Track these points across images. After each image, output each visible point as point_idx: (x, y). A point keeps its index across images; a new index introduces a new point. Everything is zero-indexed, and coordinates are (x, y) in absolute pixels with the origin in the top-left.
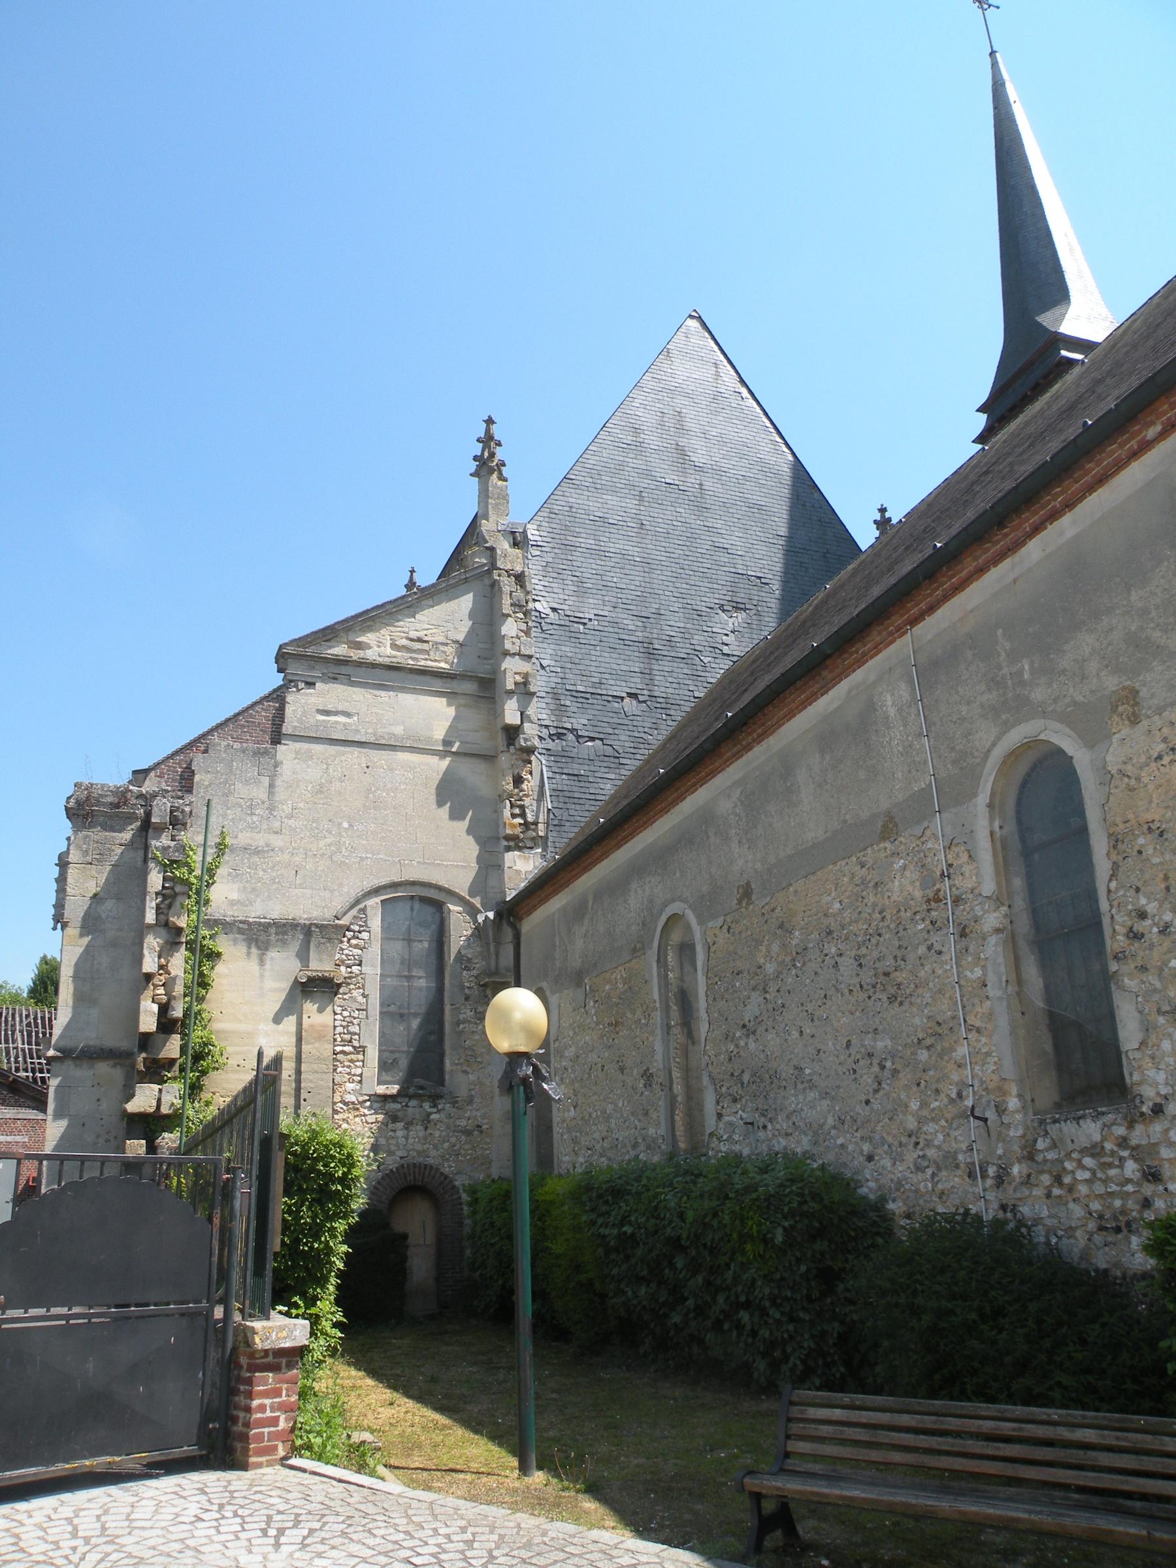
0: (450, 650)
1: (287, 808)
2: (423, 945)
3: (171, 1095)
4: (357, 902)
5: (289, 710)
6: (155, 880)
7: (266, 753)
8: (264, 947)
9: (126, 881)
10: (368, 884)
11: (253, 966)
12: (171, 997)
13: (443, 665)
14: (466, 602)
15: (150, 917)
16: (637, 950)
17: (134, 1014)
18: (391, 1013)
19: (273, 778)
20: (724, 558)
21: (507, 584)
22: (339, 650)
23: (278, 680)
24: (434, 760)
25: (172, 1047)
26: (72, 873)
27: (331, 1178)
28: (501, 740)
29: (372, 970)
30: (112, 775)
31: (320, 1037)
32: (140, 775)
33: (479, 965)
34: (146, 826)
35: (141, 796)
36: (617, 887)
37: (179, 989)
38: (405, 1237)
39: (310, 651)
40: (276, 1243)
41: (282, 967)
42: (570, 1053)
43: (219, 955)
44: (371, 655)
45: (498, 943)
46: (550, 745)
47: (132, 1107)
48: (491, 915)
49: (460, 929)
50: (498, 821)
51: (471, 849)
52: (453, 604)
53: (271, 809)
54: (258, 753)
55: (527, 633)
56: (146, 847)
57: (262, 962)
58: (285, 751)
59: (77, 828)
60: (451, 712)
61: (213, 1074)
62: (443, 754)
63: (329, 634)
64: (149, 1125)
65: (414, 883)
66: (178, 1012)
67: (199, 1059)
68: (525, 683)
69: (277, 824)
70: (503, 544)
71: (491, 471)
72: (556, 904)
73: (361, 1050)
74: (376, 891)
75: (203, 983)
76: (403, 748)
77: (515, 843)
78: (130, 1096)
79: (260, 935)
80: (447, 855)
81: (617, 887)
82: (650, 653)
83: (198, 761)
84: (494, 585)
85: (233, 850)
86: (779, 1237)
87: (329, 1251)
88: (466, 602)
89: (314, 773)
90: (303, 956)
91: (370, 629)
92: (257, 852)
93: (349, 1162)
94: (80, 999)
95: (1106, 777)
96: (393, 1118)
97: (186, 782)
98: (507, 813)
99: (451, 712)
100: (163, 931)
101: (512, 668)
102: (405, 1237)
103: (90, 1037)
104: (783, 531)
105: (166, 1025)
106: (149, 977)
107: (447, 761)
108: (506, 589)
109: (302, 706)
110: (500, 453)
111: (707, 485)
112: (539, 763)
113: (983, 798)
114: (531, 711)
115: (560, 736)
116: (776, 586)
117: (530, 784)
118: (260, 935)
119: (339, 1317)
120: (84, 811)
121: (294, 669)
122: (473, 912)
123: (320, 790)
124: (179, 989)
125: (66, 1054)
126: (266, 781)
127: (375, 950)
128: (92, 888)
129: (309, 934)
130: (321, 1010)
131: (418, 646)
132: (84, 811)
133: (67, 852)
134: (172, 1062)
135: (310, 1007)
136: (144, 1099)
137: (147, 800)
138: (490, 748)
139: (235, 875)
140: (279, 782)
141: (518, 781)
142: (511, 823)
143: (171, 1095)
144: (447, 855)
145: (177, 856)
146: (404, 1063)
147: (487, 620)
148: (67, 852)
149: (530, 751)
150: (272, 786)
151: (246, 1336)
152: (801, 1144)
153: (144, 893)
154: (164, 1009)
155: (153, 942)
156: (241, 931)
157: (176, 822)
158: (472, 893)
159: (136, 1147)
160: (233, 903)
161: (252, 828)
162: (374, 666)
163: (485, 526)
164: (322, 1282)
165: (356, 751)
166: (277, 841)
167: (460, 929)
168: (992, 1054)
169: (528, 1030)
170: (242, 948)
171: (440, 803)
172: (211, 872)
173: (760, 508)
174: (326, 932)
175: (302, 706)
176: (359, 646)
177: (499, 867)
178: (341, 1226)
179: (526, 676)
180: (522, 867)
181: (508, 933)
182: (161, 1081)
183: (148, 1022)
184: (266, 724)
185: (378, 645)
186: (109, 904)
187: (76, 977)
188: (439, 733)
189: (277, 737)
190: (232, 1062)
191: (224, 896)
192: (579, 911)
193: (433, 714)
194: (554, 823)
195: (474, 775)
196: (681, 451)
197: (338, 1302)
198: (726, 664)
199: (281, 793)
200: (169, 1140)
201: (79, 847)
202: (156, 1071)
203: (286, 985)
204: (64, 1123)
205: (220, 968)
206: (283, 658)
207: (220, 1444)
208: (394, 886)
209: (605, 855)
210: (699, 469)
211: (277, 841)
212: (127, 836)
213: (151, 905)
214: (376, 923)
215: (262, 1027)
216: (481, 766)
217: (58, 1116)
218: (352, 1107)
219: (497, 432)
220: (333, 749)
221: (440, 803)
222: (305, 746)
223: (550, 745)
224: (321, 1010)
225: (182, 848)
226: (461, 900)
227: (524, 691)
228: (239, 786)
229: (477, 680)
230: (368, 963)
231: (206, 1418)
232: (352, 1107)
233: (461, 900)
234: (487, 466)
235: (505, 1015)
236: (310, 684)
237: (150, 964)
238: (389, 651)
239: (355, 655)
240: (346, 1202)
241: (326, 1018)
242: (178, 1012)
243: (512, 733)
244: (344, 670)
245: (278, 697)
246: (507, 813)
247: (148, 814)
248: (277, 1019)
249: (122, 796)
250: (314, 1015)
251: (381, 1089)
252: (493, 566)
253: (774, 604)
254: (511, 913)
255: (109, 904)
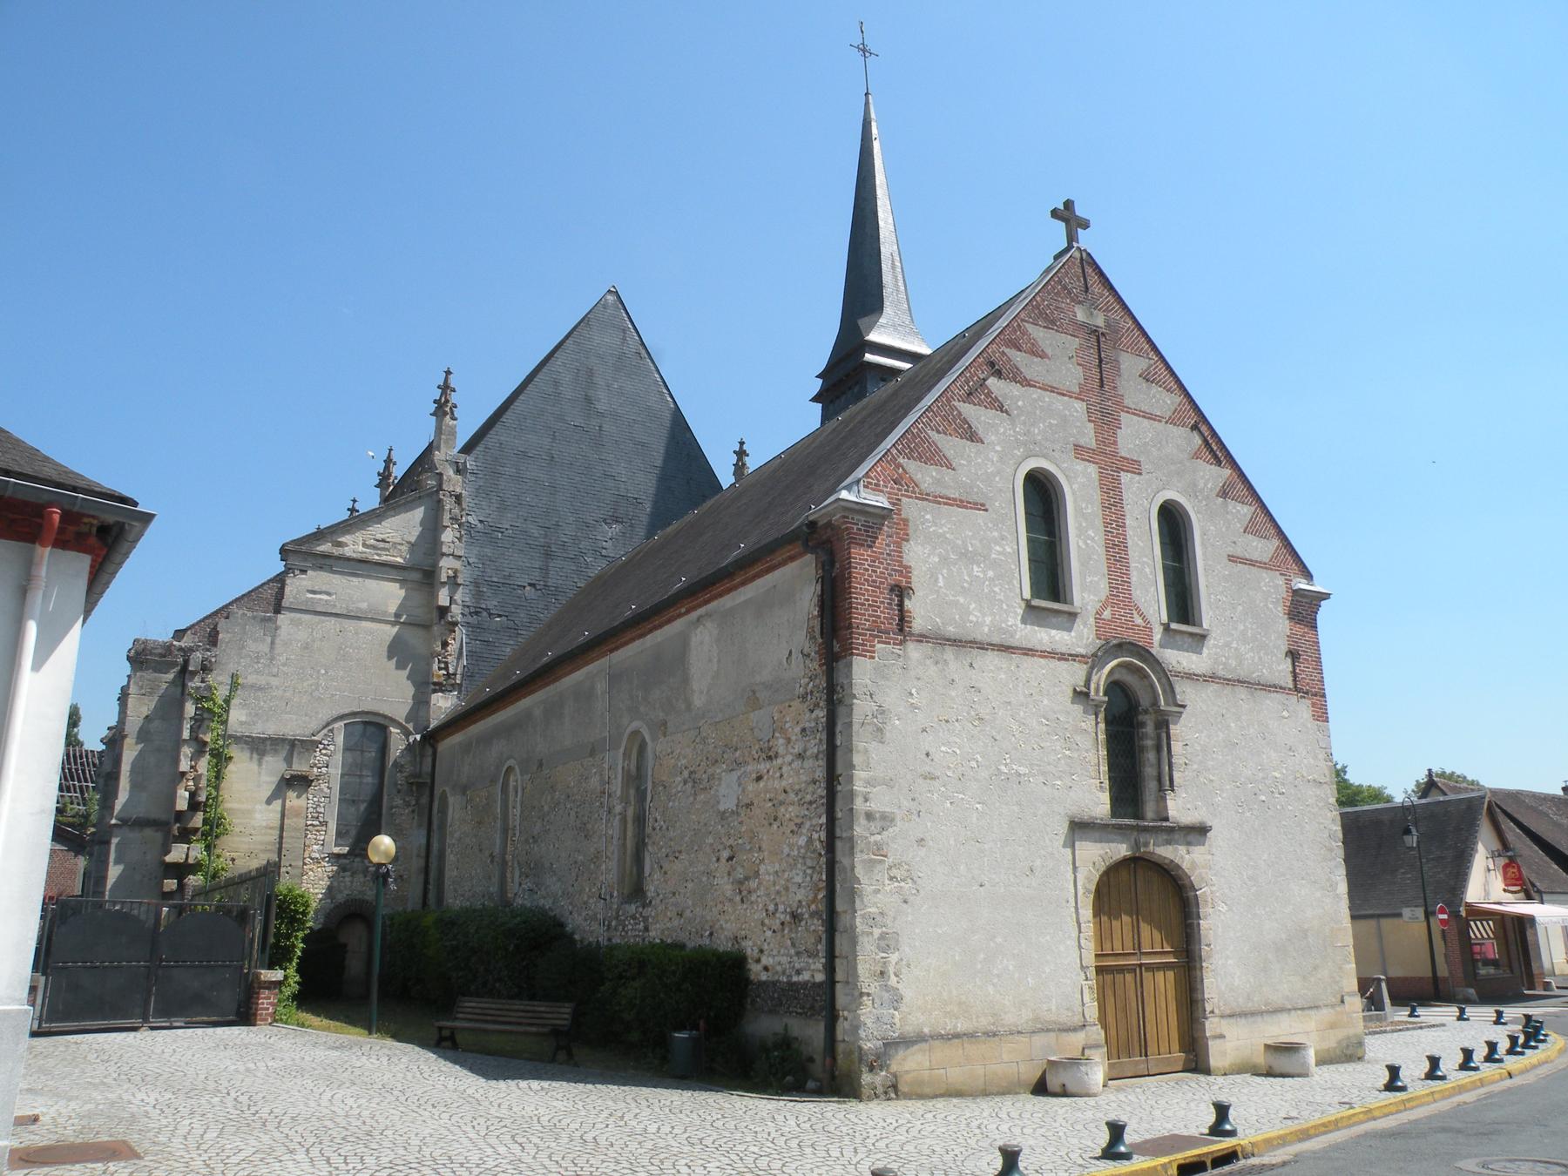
0: (404, 548)
1: (283, 659)
2: (372, 754)
3: (197, 851)
4: (328, 724)
5: (287, 590)
6: (190, 709)
7: (269, 619)
8: (262, 754)
9: (170, 708)
10: (335, 713)
11: (254, 766)
12: (198, 788)
13: (399, 560)
14: (419, 513)
15: (186, 734)
16: (493, 781)
17: (172, 797)
18: (346, 800)
19: (274, 638)
20: (611, 484)
21: (449, 503)
22: (325, 547)
23: (280, 567)
24: (388, 627)
25: (198, 820)
26: (131, 701)
27: (296, 912)
28: (435, 614)
29: (336, 771)
30: (161, 634)
31: (297, 815)
32: (179, 634)
33: (408, 769)
34: (184, 672)
35: (181, 649)
36: (486, 740)
37: (203, 783)
38: (345, 946)
39: (304, 548)
40: (272, 940)
41: (274, 767)
42: (457, 835)
43: (231, 758)
44: (347, 552)
45: (422, 756)
46: (470, 619)
47: (168, 859)
48: (418, 737)
49: (398, 744)
50: (429, 672)
51: (410, 690)
52: (409, 515)
53: (272, 659)
54: (264, 620)
55: (459, 539)
56: (184, 686)
57: (260, 764)
58: (283, 619)
59: (134, 669)
60: (402, 593)
61: (224, 838)
62: (394, 624)
63: (320, 535)
64: (181, 870)
65: (367, 713)
66: (202, 798)
67: (213, 831)
68: (455, 577)
69: (275, 670)
70: (450, 472)
71: (445, 414)
72: (457, 739)
73: (325, 824)
74: (341, 718)
75: (219, 776)
76: (366, 619)
77: (440, 688)
78: (168, 852)
79: (259, 746)
80: (391, 694)
81: (486, 740)
82: (548, 555)
83: (222, 625)
84: (440, 501)
85: (243, 687)
86: (511, 948)
87: (294, 946)
88: (419, 513)
89: (302, 635)
90: (289, 760)
91: (348, 532)
92: (260, 689)
93: (306, 905)
94: (135, 786)
95: (656, 757)
96: (343, 869)
97: (213, 639)
98: (435, 666)
99: (402, 593)
100: (194, 743)
101: (446, 565)
102: (345, 946)
103: (139, 812)
104: (659, 463)
105: (194, 805)
106: (183, 774)
107: (396, 629)
108: (447, 507)
109: (297, 587)
110: (454, 398)
111: (605, 427)
112: (461, 633)
113: (622, 750)
114: (458, 597)
115: (477, 613)
116: (648, 507)
117: (453, 647)
118: (259, 746)
119: (297, 978)
120: (141, 657)
121: (295, 561)
122: (407, 733)
123: (306, 647)
124: (203, 783)
125: (125, 822)
126: (269, 639)
127: (339, 757)
128: (145, 711)
129: (294, 746)
130: (298, 797)
131: (381, 545)
132: (141, 657)
133: (128, 685)
134: (197, 830)
135: (291, 794)
136: (177, 854)
137: (186, 652)
138: (426, 620)
139: (244, 706)
140: (277, 641)
141: (445, 644)
142: (438, 674)
143: (197, 851)
144: (391, 694)
145: (205, 694)
146: (353, 832)
147: (432, 528)
148: (128, 685)
149: (455, 624)
150: (273, 643)
151: (257, 976)
152: (547, 904)
153: (181, 717)
154: (193, 795)
155: (187, 751)
156: (246, 743)
157: (206, 668)
158: (407, 720)
159: (171, 884)
160: (242, 723)
161: (258, 672)
162: (349, 559)
163: (438, 456)
164: (290, 961)
165: (333, 620)
166: (275, 682)
167: (398, 744)
168: (609, 873)
169: (386, 853)
170: (247, 754)
171: (390, 658)
172: (227, 701)
173: (643, 445)
174: (306, 746)
175: (297, 587)
176: (340, 544)
177: (428, 703)
178: (300, 934)
179: (456, 572)
180: (443, 704)
181: (429, 751)
182: (189, 842)
183: (182, 804)
184: (270, 599)
185: (354, 545)
186: (156, 724)
187: (132, 771)
188: (393, 609)
189: (278, 610)
190: (237, 829)
191: (237, 717)
192: (467, 748)
193: (390, 595)
194: (468, 675)
195: (415, 638)
196: (588, 400)
197: (297, 971)
198: (604, 564)
199: (279, 648)
200: (195, 880)
201: (136, 683)
202: (186, 836)
203: (276, 779)
204: (121, 867)
205: (231, 767)
206: (284, 552)
207: (244, 1016)
208: (354, 714)
209: (482, 718)
210: (602, 415)
211: (275, 682)
212: (170, 676)
213: (187, 727)
214: (340, 739)
215: (258, 807)
216: (420, 632)
217: (117, 862)
218: (316, 861)
219: (453, 382)
220: (317, 618)
221: (390, 658)
222: (298, 615)
223: (470, 619)
224: (298, 797)
225: (209, 688)
226: (399, 725)
227: (453, 582)
228: (250, 642)
229: (421, 572)
230: (330, 764)
231: (239, 1006)
232: (316, 861)
233: (399, 725)
234: (443, 409)
235: (377, 847)
236: (304, 571)
237: (184, 765)
238: (361, 548)
239: (336, 551)
240: (304, 923)
241: (302, 802)
242: (202, 798)
243: (444, 611)
244: (328, 562)
245: (280, 580)
246: (435, 666)
247: (186, 663)
248: (269, 802)
249: (168, 648)
250: (293, 800)
251: (336, 850)
252: (440, 488)
253: (645, 519)
254: (432, 738)
255: (156, 724)
